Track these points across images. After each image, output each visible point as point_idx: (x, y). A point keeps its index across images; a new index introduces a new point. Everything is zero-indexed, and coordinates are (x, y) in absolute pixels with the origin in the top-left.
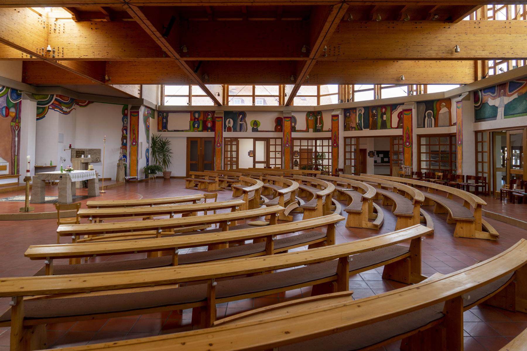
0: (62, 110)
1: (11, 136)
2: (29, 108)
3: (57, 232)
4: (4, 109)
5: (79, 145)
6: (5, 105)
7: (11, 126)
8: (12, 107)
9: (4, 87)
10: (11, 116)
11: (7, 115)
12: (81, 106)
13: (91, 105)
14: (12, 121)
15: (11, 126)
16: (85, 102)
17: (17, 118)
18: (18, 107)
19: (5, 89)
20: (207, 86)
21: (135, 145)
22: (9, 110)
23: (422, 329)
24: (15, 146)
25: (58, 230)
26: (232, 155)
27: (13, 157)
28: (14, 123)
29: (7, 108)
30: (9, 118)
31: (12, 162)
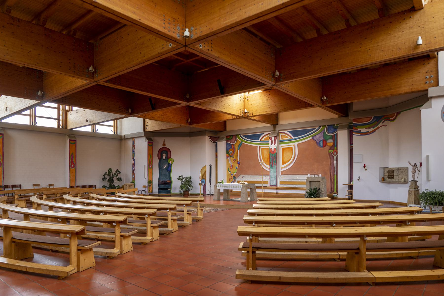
0: (360, 132)
1: (329, 160)
2: (342, 136)
3: (238, 232)
4: (321, 142)
5: (392, 165)
6: (323, 139)
7: (329, 153)
8: (330, 138)
9: (320, 127)
10: (328, 146)
11: (324, 146)
12: (392, 120)
13: (399, 116)
14: (330, 149)
15: (329, 153)
16: (371, 118)
17: (335, 146)
18: (335, 138)
19: (321, 128)
20: (170, 46)
21: (73, 167)
22: (326, 142)
23: (73, 75)
24: (334, 168)
25: (238, 230)
26: (206, 192)
27: (332, 175)
28: (332, 151)
29: (325, 141)
30: (327, 148)
31: (331, 180)
